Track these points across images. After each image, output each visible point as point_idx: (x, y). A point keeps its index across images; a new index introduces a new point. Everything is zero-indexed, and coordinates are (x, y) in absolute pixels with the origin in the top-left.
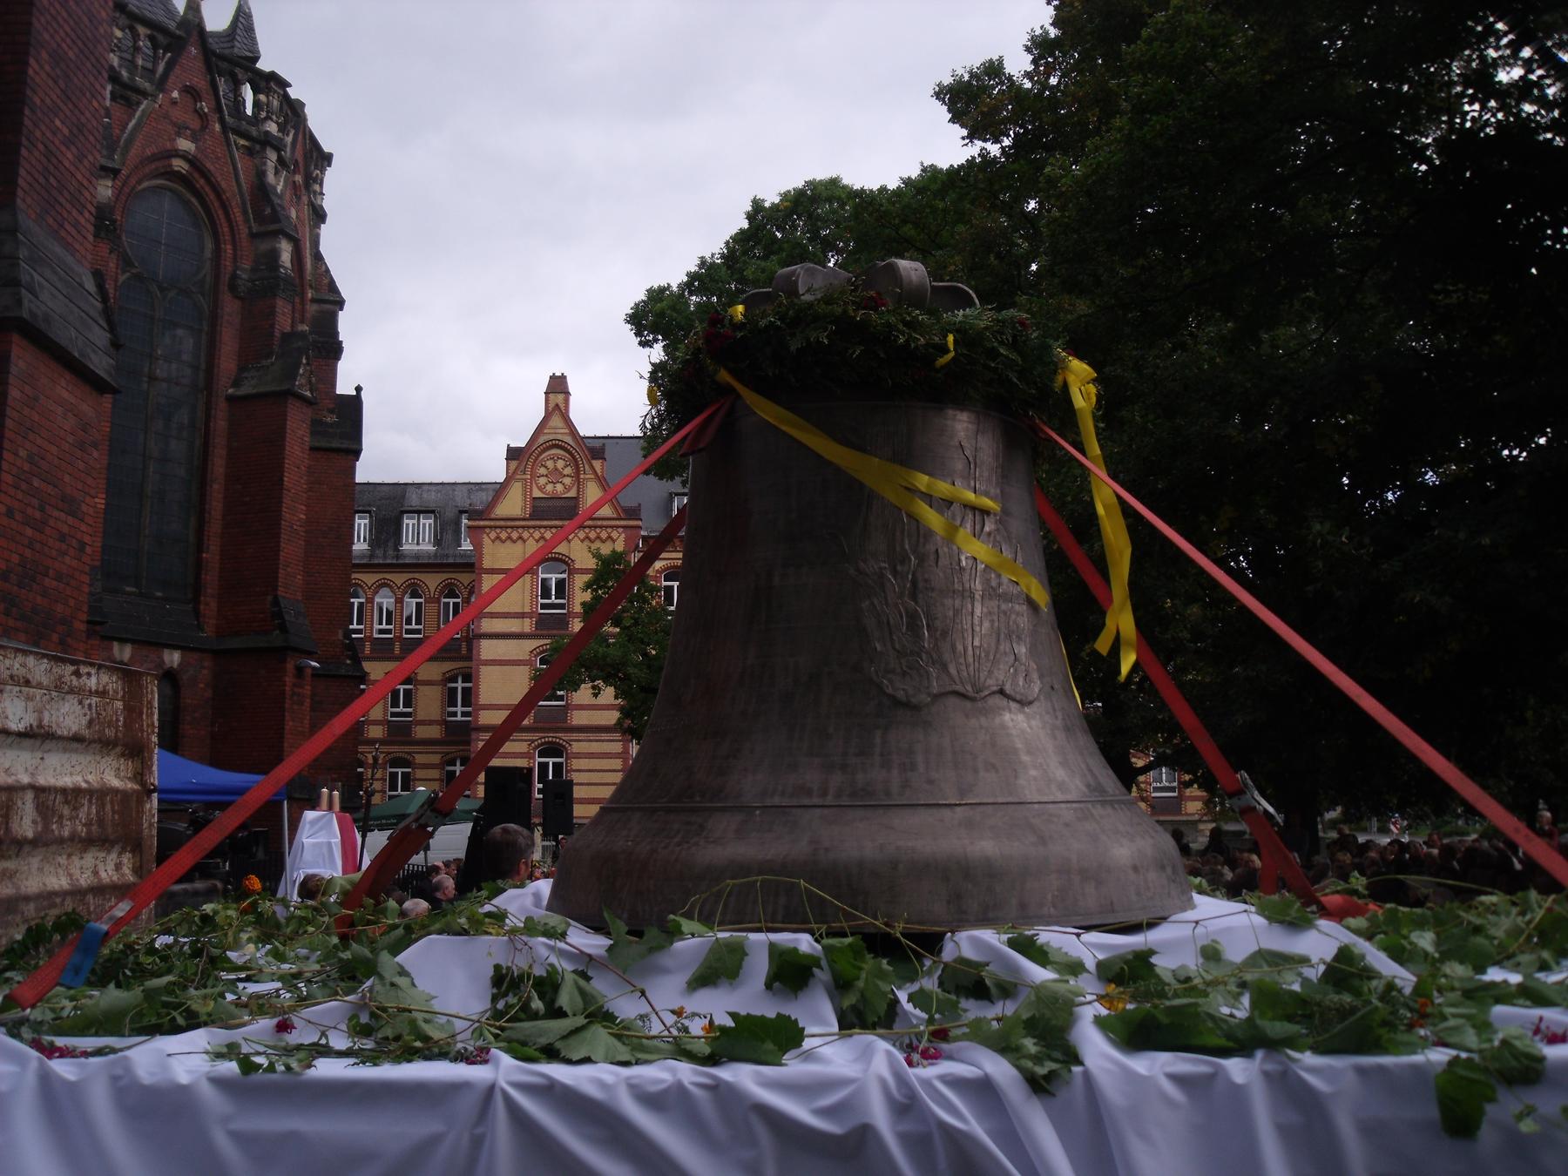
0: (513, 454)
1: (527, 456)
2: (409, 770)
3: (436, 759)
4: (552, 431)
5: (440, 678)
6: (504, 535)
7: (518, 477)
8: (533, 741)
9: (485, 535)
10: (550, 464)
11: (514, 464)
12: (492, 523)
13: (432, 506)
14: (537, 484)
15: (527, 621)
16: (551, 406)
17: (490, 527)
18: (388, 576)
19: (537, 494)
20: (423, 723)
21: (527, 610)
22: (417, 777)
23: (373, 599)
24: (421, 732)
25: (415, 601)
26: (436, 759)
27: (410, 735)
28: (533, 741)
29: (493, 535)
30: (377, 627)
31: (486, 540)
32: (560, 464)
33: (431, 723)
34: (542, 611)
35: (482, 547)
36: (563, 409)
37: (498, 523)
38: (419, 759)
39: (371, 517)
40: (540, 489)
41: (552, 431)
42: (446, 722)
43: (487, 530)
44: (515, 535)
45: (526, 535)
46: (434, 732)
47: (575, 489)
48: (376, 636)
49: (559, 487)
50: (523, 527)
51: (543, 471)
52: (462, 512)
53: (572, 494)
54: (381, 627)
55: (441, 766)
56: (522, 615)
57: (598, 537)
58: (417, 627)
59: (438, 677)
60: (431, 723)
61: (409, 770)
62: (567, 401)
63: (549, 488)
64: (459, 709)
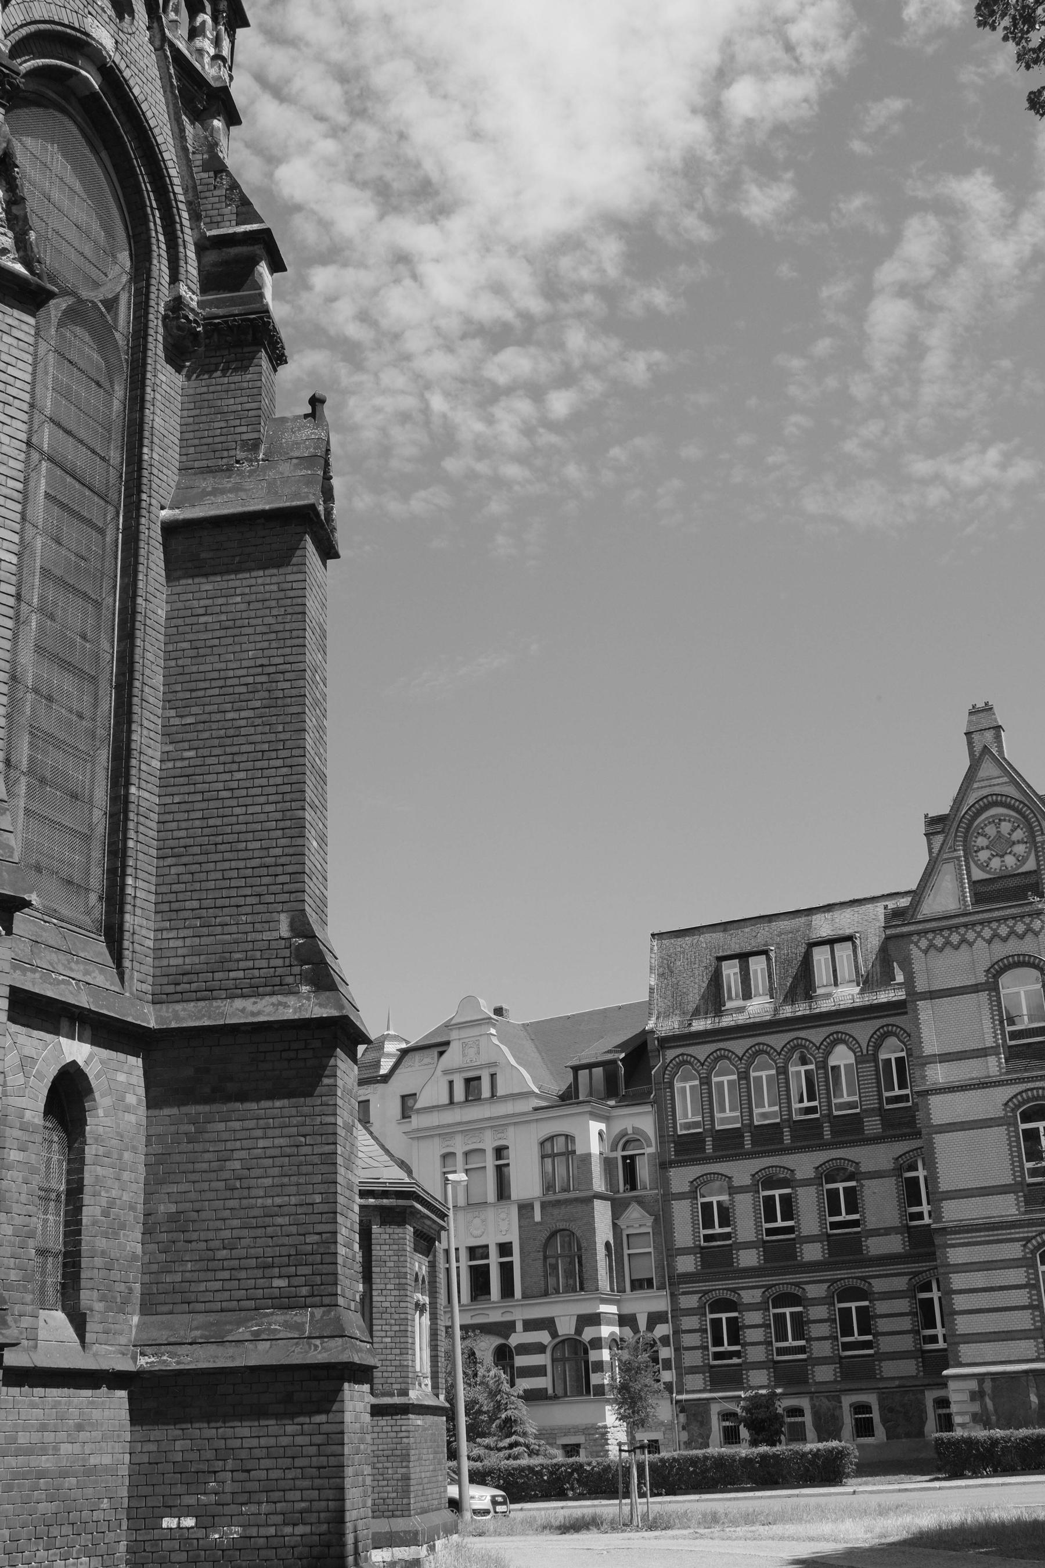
0: (936, 825)
1: (955, 825)
2: (866, 1303)
3: (901, 1283)
4: (983, 784)
5: (891, 1166)
6: (939, 941)
7: (945, 856)
8: (1028, 1240)
9: (912, 946)
10: (991, 830)
11: (938, 840)
12: (920, 927)
13: (848, 932)
14: (976, 863)
15: (992, 1060)
16: (978, 749)
17: (918, 933)
18: (802, 1034)
19: (978, 875)
20: (876, 1233)
21: (989, 1042)
22: (747, 1322)
23: (825, 1062)
24: (875, 1246)
25: (802, 1069)
26: (901, 1283)
27: (794, 1257)
28: (1028, 1240)
29: (924, 943)
30: (796, 1106)
31: (915, 953)
32: (1006, 827)
33: (887, 1231)
34: (1013, 1043)
35: (911, 964)
36: (994, 751)
37: (928, 926)
38: (879, 1285)
39: (769, 959)
40: (984, 867)
41: (983, 784)
42: (909, 1228)
43: (915, 938)
44: (955, 938)
45: (971, 935)
46: (894, 1244)
47: (1032, 857)
48: (796, 1117)
49: (1010, 860)
50: (965, 925)
51: (981, 841)
52: (721, 959)
53: (1030, 865)
54: (801, 1105)
55: (910, 1293)
56: (982, 1053)
57: (1012, 932)
58: (851, 1099)
59: (887, 1165)
60: (887, 1231)
61: (866, 1303)
62: (998, 738)
63: (996, 863)
64: (925, 1208)
